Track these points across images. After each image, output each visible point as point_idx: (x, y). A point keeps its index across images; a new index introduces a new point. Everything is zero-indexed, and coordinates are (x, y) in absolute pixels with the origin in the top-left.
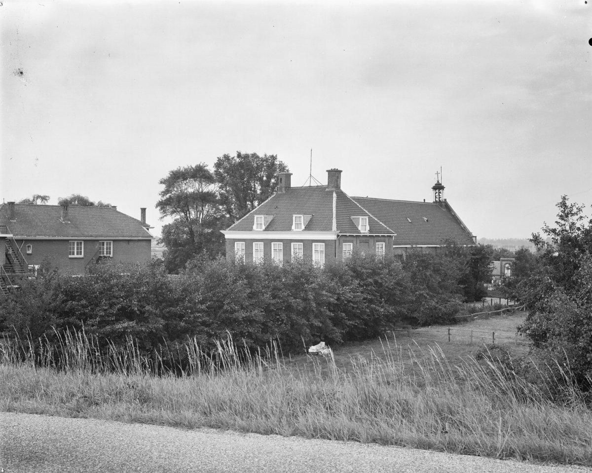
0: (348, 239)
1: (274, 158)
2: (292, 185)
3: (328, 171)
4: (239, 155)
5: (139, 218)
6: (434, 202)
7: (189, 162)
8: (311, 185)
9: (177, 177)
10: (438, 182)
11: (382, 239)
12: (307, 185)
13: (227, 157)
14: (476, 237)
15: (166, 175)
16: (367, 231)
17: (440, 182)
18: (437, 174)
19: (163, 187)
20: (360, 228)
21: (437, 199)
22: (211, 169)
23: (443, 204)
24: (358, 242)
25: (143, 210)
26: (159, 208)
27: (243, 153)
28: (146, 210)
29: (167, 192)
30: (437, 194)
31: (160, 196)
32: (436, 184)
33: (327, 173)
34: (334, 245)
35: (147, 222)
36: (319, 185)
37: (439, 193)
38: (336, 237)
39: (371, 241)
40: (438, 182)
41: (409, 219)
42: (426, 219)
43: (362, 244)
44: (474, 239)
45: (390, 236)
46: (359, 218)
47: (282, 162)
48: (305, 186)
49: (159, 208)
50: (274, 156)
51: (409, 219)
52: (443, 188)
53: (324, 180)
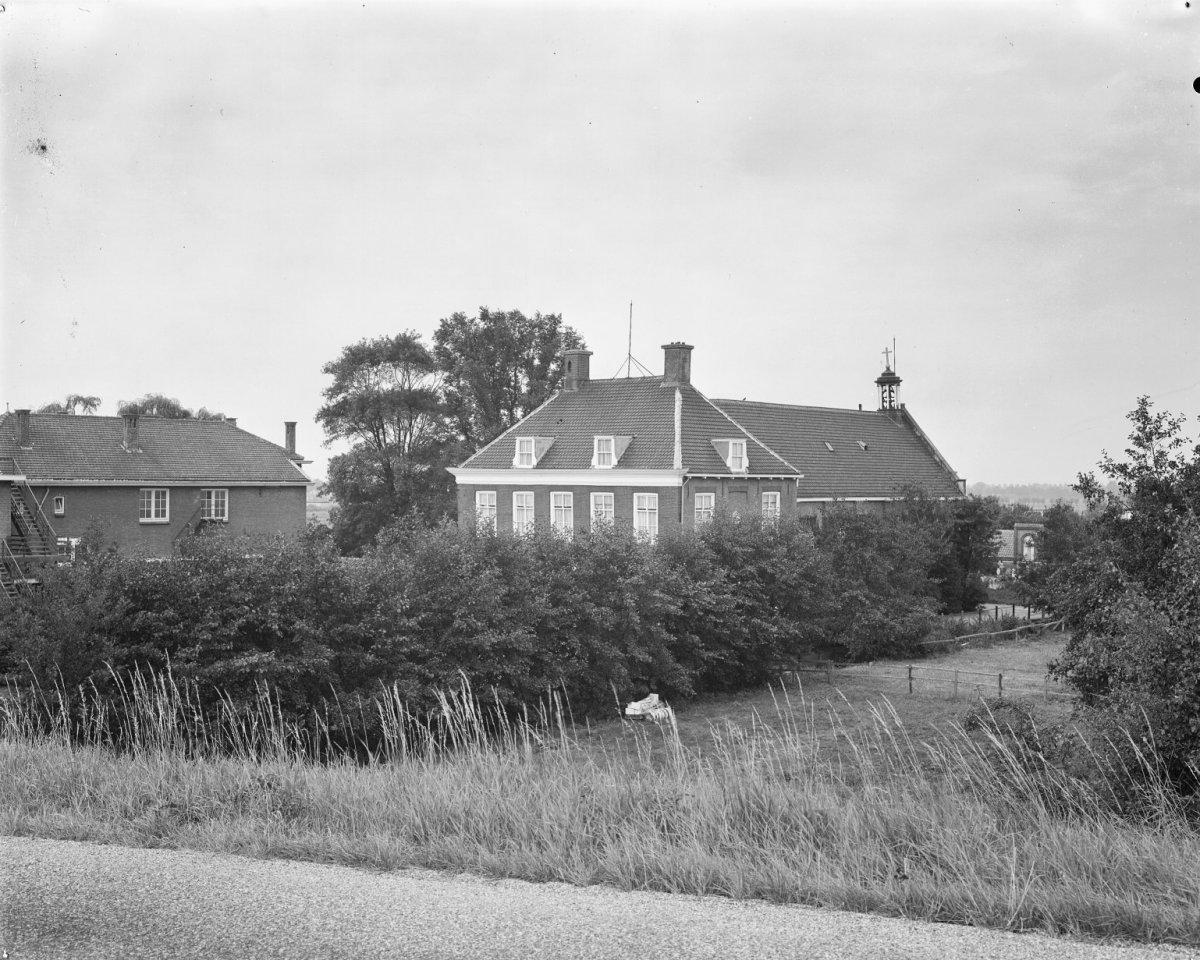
0: (705, 485)
1: (555, 320)
2: (593, 376)
3: (665, 347)
4: (485, 316)
5: (281, 442)
6: (879, 410)
7: (382, 329)
8: (631, 376)
9: (359, 358)
10: (888, 369)
11: (775, 484)
12: (623, 375)
13: (459, 319)
14: (964, 481)
15: (337, 355)
16: (744, 469)
17: (892, 370)
18: (887, 352)
19: (330, 380)
20: (729, 463)
21: (887, 405)
22: (428, 343)
23: (899, 414)
24: (726, 491)
25: (291, 427)
26: (322, 422)
27: (493, 310)
28: (297, 427)
29: (338, 389)
30: (886, 394)
31: (325, 398)
32: (883, 374)
33: (663, 351)
34: (677, 497)
35: (299, 451)
36: (647, 374)
37: (890, 391)
38: (681, 480)
39: (752, 489)
40: (888, 369)
41: (828, 445)
42: (864, 444)
43: (734, 494)
44: (961, 484)
45: (791, 479)
46: (728, 443)
47: (571, 328)
48: (618, 377)
49: (322, 422)
50: (556, 316)
51: (828, 445)
52: (897, 381)
53: (656, 366)
